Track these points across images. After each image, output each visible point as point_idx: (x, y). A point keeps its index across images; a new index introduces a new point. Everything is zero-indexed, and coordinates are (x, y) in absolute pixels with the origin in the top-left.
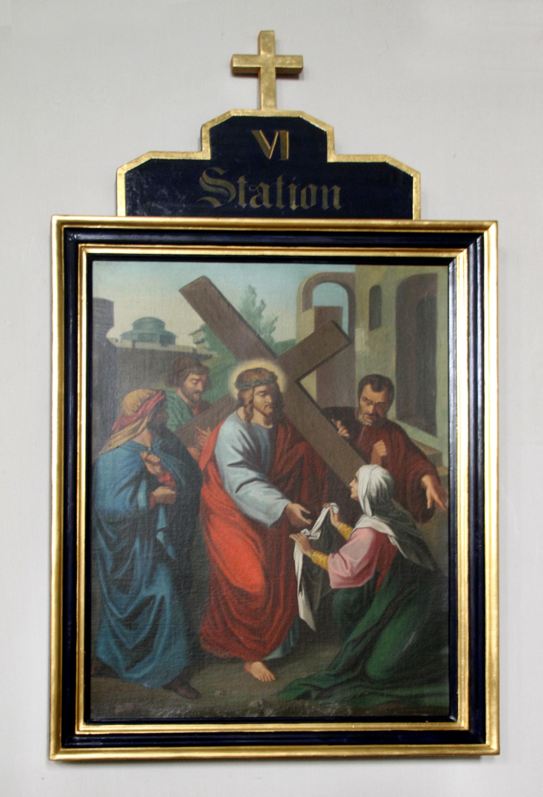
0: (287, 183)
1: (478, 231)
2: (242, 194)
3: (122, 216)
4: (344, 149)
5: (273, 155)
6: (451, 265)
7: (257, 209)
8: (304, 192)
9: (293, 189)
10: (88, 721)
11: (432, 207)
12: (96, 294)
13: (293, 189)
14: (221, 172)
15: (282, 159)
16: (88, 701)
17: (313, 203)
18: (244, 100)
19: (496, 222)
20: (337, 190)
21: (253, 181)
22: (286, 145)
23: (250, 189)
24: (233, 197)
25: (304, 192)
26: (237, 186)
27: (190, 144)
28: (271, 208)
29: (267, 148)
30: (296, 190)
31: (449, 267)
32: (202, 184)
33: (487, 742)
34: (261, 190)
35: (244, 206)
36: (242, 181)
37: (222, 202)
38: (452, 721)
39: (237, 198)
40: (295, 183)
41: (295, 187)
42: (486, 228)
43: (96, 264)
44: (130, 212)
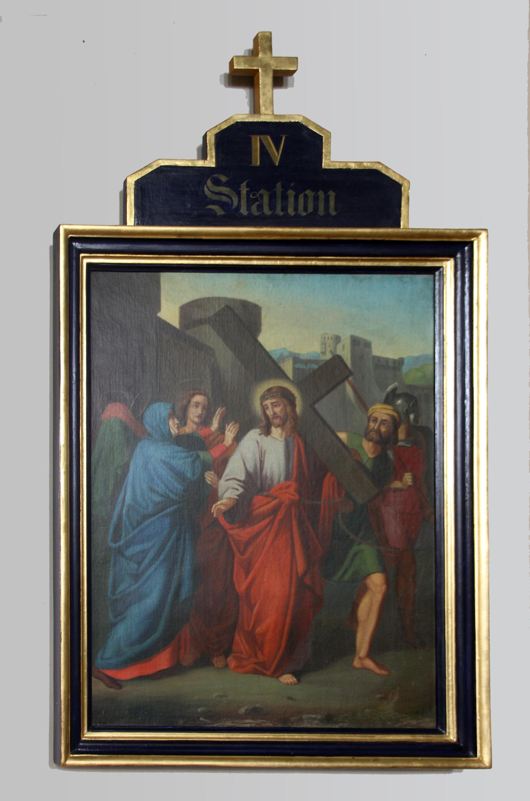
0: (285, 188)
3: (131, 225)
4: (339, 154)
5: (260, 162)
6: (437, 273)
8: (301, 201)
11: (419, 216)
13: (291, 193)
14: (224, 179)
15: (252, 165)
16: (92, 717)
18: (235, 107)
19: (486, 230)
20: (332, 194)
24: (235, 204)
26: (239, 194)
27: (184, 150)
29: (275, 155)
30: (240, 209)
31: (435, 277)
32: (206, 189)
34: (261, 196)
36: (244, 190)
38: (442, 734)
39: (239, 207)
40: (292, 188)
41: (294, 193)
42: (477, 235)
43: (93, 274)
44: (141, 220)
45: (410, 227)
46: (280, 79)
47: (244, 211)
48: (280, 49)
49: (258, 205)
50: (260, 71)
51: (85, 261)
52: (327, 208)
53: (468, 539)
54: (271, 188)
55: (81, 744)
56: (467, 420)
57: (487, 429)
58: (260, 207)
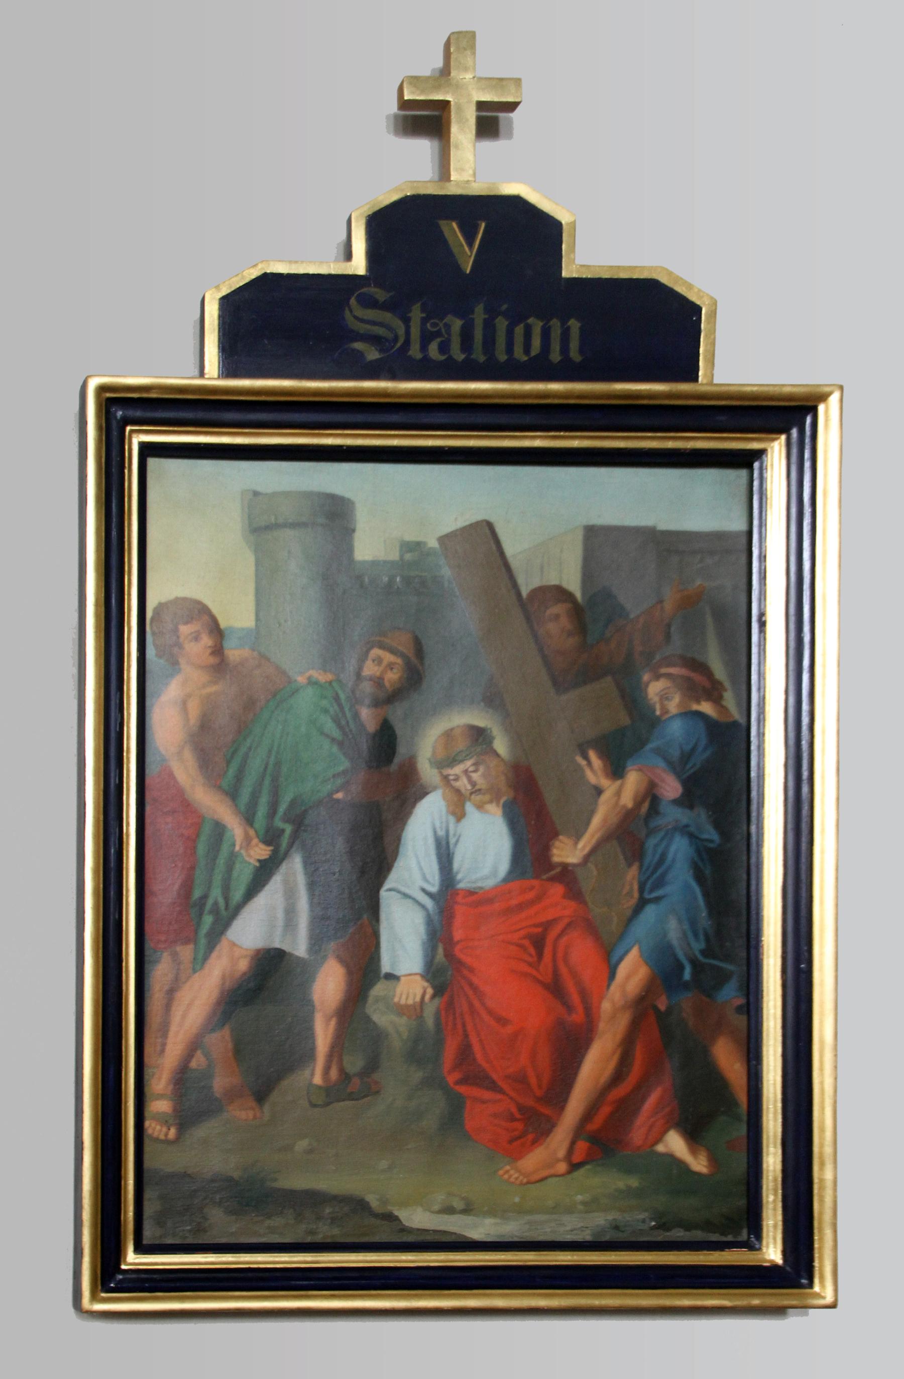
0: (492, 313)
1: (809, 404)
2: (415, 332)
3: (212, 374)
4: (588, 255)
7: (441, 362)
8: (519, 330)
9: (502, 324)
10: (140, 1249)
11: (733, 362)
13: (502, 324)
16: (145, 1229)
18: (408, 168)
20: (574, 325)
22: (481, 242)
23: (428, 325)
25: (519, 330)
26: (407, 321)
33: (817, 1288)
34: (448, 326)
35: (419, 356)
36: (416, 314)
37: (381, 351)
39: (407, 342)
43: (153, 463)
44: (229, 369)
45: (715, 382)
46: (490, 122)
47: (415, 352)
49: (442, 342)
51: (136, 440)
52: (565, 350)
53: (803, 912)
54: (465, 313)
55: (121, 1277)
56: (805, 707)
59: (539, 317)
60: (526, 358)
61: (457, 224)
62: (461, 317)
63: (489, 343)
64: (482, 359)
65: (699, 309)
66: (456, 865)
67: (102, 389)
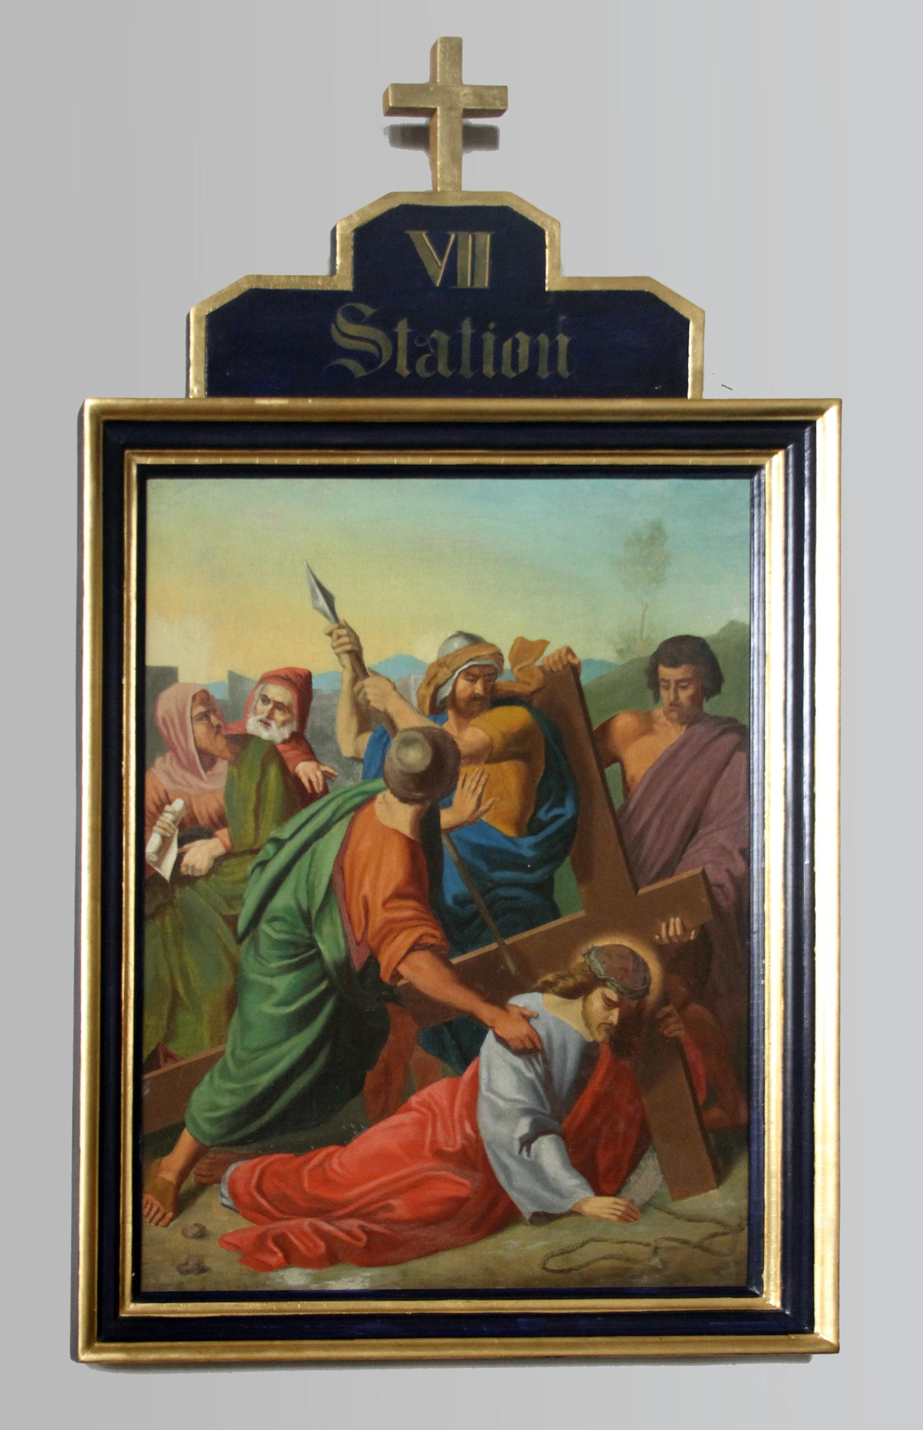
0: (480, 328)
4: (576, 261)
7: (428, 379)
8: (507, 345)
9: (489, 339)
11: (724, 373)
12: (152, 660)
13: (489, 339)
17: (524, 366)
18: (410, 176)
20: (563, 340)
21: (419, 330)
24: (386, 356)
25: (507, 345)
26: (394, 338)
27: (308, 253)
28: (452, 376)
34: (435, 343)
36: (403, 329)
40: (494, 331)
42: (820, 412)
43: (153, 484)
44: (215, 387)
45: (705, 396)
48: (476, 72)
49: (428, 359)
50: (438, 113)
52: (515, 365)
57: (839, 980)
58: (432, 364)
59: (527, 332)
60: (514, 375)
61: (428, 235)
62: (446, 329)
63: (477, 361)
64: (406, 372)
65: (686, 323)
66: (733, 760)
67: (97, 414)
